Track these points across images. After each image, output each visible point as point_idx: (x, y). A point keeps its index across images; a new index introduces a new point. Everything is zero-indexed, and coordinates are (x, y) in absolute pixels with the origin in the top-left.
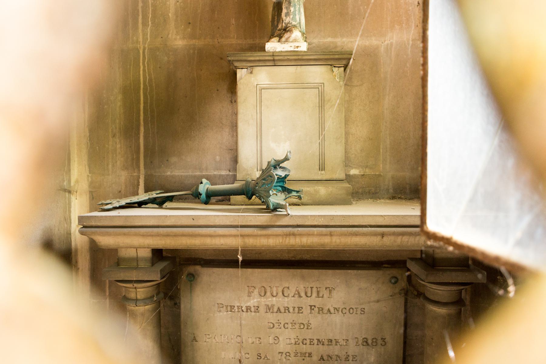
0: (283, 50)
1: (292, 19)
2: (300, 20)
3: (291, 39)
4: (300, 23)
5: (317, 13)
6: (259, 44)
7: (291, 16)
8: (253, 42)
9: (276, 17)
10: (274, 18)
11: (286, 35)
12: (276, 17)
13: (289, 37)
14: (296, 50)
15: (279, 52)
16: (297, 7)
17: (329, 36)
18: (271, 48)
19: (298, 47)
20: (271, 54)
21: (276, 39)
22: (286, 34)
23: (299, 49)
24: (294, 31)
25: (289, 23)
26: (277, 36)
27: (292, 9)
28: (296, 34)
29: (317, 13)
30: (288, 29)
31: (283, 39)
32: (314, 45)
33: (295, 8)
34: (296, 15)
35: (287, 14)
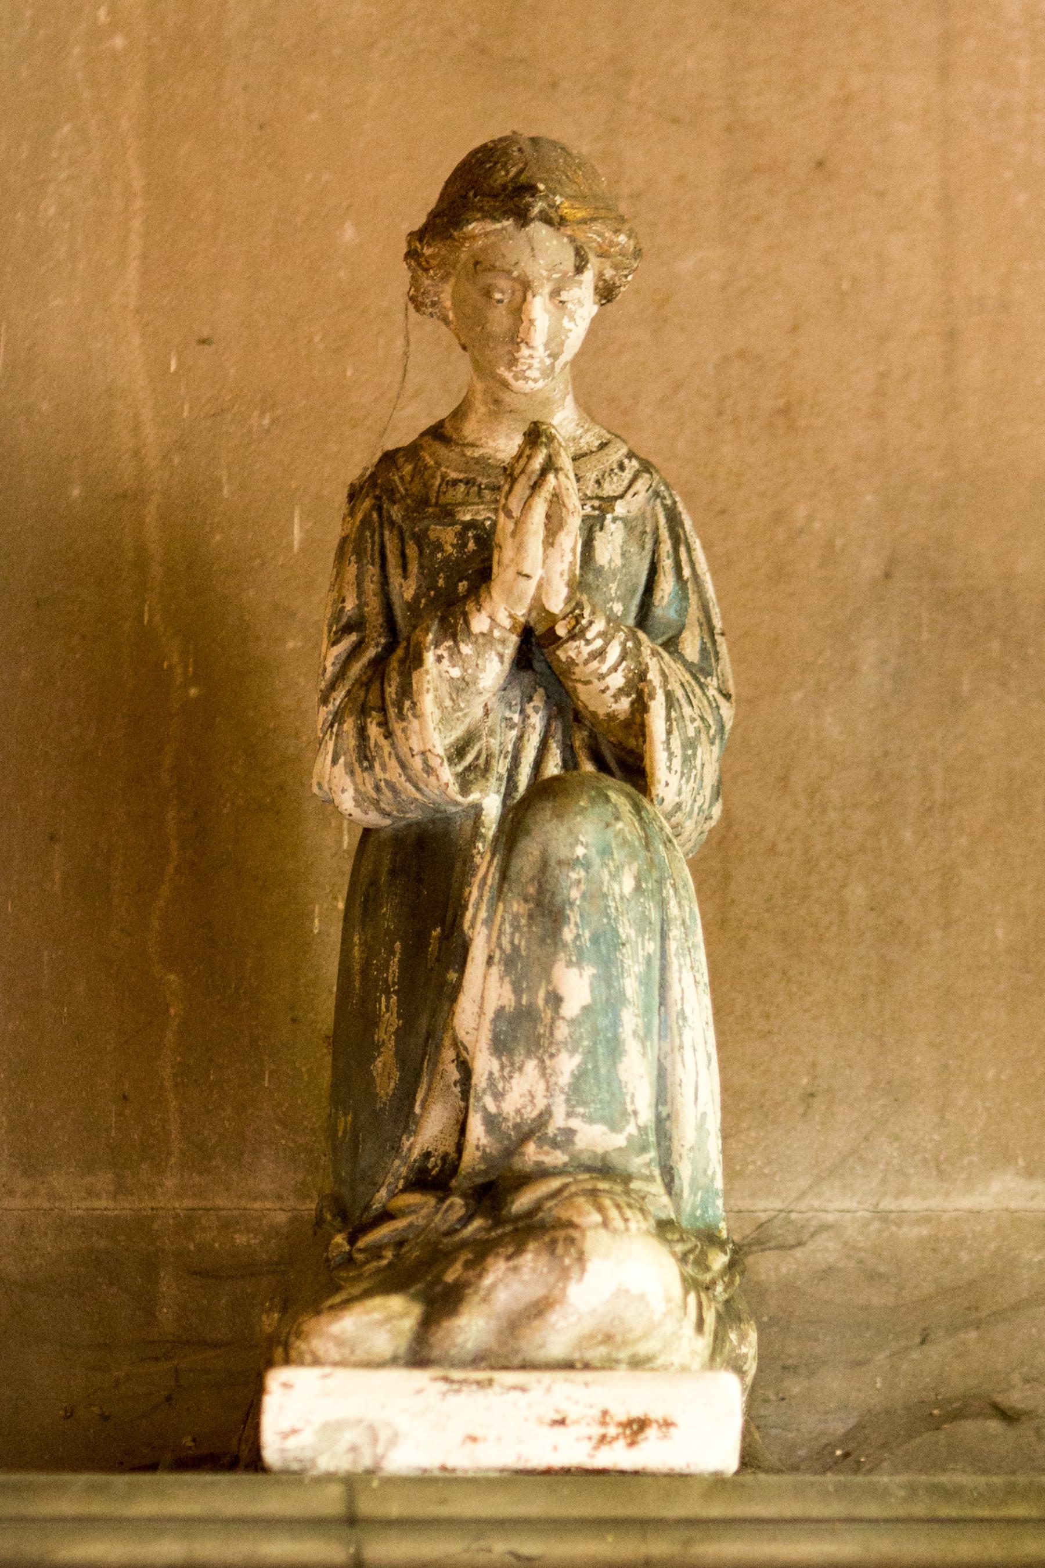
0: (465, 1460)
1: (576, 1092)
2: (663, 1093)
3: (557, 1336)
4: (663, 1129)
5: (857, 894)
6: (187, 1224)
7: (567, 1064)
8: (125, 1207)
9: (389, 1013)
10: (372, 1021)
11: (506, 1284)
12: (389, 1013)
13: (538, 1309)
14: (618, 1456)
15: (424, 1481)
16: (637, 954)
17: (1002, 1157)
18: (331, 1429)
19: (636, 1428)
20: (329, 1502)
21: (380, 1321)
22: (497, 1270)
23: (651, 1454)
24: (596, 1241)
25: (534, 1130)
26: (392, 1282)
27: (576, 986)
28: (622, 1273)
29: (857, 894)
30: (523, 1201)
31: (471, 1327)
32: (825, 1251)
33: (608, 976)
34: (615, 1049)
35: (522, 1031)
